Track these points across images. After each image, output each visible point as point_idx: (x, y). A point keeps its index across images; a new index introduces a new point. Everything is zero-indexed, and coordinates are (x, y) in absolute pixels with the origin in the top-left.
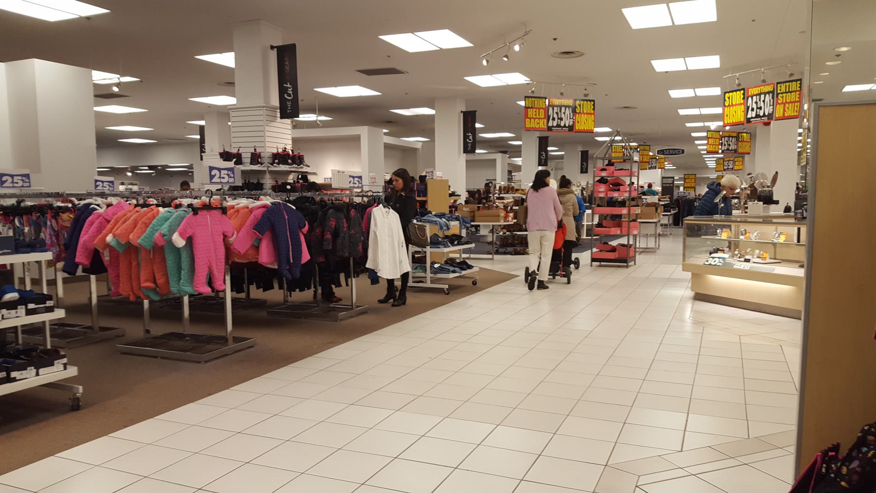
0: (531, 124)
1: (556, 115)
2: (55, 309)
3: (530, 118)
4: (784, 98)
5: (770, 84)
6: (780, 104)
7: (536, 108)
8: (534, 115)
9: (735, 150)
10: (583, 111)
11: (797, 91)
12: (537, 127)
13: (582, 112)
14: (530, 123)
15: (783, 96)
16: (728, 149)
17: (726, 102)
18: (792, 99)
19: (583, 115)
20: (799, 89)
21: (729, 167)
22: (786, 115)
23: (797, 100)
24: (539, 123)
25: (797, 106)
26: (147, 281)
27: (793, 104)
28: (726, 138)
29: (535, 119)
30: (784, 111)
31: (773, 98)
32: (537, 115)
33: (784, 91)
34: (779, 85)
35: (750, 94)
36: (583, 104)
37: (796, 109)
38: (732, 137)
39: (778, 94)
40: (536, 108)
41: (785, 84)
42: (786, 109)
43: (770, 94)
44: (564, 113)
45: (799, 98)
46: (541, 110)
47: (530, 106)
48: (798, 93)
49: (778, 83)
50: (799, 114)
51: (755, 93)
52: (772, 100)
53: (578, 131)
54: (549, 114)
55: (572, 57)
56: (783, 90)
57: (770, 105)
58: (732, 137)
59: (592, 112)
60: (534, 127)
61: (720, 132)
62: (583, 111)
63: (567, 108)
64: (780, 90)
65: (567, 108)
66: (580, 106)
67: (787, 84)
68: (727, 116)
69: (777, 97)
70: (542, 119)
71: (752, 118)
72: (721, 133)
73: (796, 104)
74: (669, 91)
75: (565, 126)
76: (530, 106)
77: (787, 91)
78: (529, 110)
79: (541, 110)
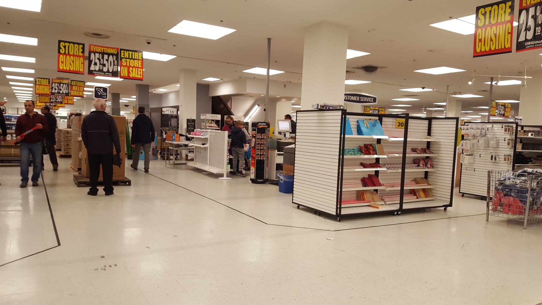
1: (98, 60)
2: (292, 119)
3: (74, 91)
7: (78, 86)
9: (503, 114)
11: (138, 68)
12: (78, 95)
14: (74, 93)
15: (127, 61)
16: (499, 114)
21: (58, 101)
23: (141, 66)
24: (80, 93)
25: (140, 71)
27: (137, 69)
29: (77, 91)
31: (117, 59)
33: (128, 57)
34: (122, 52)
37: (139, 73)
38: (109, 55)
39: (121, 58)
40: (78, 86)
43: (114, 56)
45: (82, 52)
46: (81, 87)
47: (74, 85)
48: (140, 61)
49: (121, 50)
50: (143, 77)
54: (91, 59)
55: (99, 38)
56: (381, 110)
59: (48, 84)
61: (370, 107)
66: (65, 47)
67: (131, 53)
68: (62, 62)
70: (81, 91)
72: (371, 108)
73: (139, 69)
75: (63, 93)
76: (74, 85)
78: (73, 86)
79: (81, 87)
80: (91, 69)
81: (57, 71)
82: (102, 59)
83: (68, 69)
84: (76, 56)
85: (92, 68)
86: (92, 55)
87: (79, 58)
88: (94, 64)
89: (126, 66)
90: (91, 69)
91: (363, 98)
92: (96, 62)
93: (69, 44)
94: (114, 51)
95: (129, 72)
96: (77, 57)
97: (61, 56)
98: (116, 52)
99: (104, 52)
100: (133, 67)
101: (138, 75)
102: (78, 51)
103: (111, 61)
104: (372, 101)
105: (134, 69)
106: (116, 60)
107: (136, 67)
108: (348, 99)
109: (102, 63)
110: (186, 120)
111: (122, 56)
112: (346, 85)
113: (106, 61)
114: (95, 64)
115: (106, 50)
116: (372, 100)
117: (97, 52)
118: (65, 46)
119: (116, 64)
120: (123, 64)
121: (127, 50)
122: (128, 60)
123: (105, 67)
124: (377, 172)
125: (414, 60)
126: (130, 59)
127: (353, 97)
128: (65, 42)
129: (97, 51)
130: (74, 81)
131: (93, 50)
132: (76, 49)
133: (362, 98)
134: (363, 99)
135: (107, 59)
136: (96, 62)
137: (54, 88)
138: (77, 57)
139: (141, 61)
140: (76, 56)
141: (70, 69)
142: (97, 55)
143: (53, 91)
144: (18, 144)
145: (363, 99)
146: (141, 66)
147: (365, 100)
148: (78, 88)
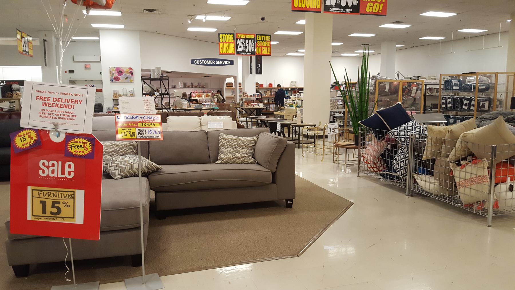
1: (242, 44)
5: (252, 35)
6: (258, 47)
10: (225, 41)
11: (268, 47)
13: (224, 41)
15: (260, 43)
17: (220, 40)
19: (225, 44)
23: (269, 46)
25: (269, 49)
27: (267, 48)
28: (241, 40)
31: (254, 42)
33: (261, 40)
34: (258, 36)
35: (238, 37)
36: (225, 36)
37: (268, 51)
39: (257, 41)
42: (263, 50)
43: (252, 40)
44: (248, 44)
45: (233, 40)
49: (257, 35)
52: (253, 44)
54: (238, 44)
58: (249, 39)
62: (225, 41)
64: (258, 39)
65: (250, 40)
66: (222, 37)
67: (263, 36)
68: (222, 48)
69: (257, 42)
73: (268, 48)
80: (238, 51)
82: (244, 43)
83: (225, 52)
84: (230, 43)
86: (238, 40)
88: (240, 47)
89: (260, 46)
90: (238, 51)
91: (219, 61)
93: (225, 35)
94: (252, 37)
97: (221, 44)
98: (253, 37)
99: (245, 38)
100: (264, 47)
101: (267, 52)
102: (230, 39)
103: (250, 44)
104: (229, 64)
105: (265, 48)
107: (266, 47)
108: (203, 63)
109: (245, 46)
110: (262, 84)
111: (257, 40)
112: (304, 49)
113: (247, 44)
116: (229, 62)
117: (242, 39)
118: (223, 36)
119: (253, 46)
122: (261, 42)
125: (196, 36)
126: (263, 41)
127: (207, 61)
128: (222, 34)
129: (241, 37)
131: (238, 37)
132: (229, 38)
133: (218, 62)
134: (219, 62)
135: (248, 42)
138: (230, 44)
140: (230, 43)
142: (241, 40)
144: (356, 116)
145: (219, 62)
146: (269, 46)
147: (221, 63)
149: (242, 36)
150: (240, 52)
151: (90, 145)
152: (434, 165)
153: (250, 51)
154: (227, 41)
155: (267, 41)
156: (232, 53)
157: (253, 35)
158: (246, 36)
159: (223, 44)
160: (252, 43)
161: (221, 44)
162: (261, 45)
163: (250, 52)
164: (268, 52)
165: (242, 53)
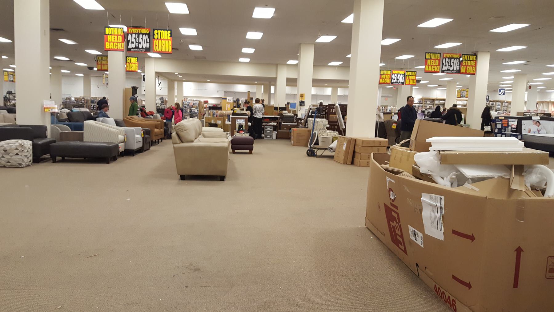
0: (111, 45)
3: (429, 65)
4: (466, 63)
6: (463, 66)
8: (431, 63)
10: (160, 38)
11: (473, 66)
17: (155, 36)
18: (430, 61)
20: (475, 60)
22: (467, 72)
23: (475, 65)
24: (387, 81)
25: (474, 68)
26: (504, 108)
27: (472, 67)
28: (447, 59)
29: (432, 66)
30: (466, 70)
32: (434, 63)
35: (444, 57)
36: (160, 33)
37: (473, 70)
38: (143, 34)
41: (467, 56)
43: (458, 59)
45: (475, 64)
49: (463, 55)
51: (447, 57)
52: (404, 77)
53: (432, 72)
54: (129, 39)
57: (457, 65)
60: (431, 70)
62: (160, 38)
63: (144, 35)
64: (464, 58)
66: (158, 34)
67: (469, 56)
70: (437, 66)
71: (132, 48)
73: (473, 67)
74: (262, 33)
75: (142, 48)
76: (110, 34)
77: (468, 59)
78: (428, 60)
81: (424, 73)
84: (166, 40)
85: (130, 46)
86: (393, 75)
87: (168, 41)
92: (133, 41)
95: (466, 70)
96: (166, 41)
98: (148, 31)
99: (139, 33)
106: (148, 38)
110: (286, 79)
114: (132, 43)
115: (140, 31)
117: (134, 33)
118: (158, 33)
119: (148, 42)
120: (463, 64)
121: (466, 55)
123: (451, 67)
124: (103, 78)
126: (468, 60)
129: (133, 32)
130: (464, 55)
132: (166, 35)
135: (453, 61)
136: (133, 41)
137: (393, 79)
139: (475, 62)
140: (166, 40)
141: (161, 50)
143: (393, 81)
146: (475, 65)
148: (433, 61)
149: (449, 56)
150: (445, 70)
151: (143, 130)
152: (83, 133)
153: (144, 47)
154: (162, 38)
155: (472, 60)
156: (168, 51)
157: (459, 55)
158: (451, 56)
159: (158, 41)
160: (458, 62)
161: (155, 41)
162: (466, 64)
163: (144, 49)
164: (473, 71)
165: (447, 71)
